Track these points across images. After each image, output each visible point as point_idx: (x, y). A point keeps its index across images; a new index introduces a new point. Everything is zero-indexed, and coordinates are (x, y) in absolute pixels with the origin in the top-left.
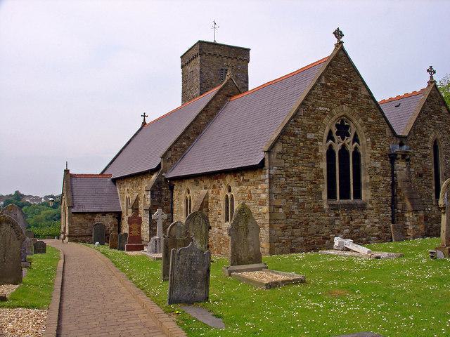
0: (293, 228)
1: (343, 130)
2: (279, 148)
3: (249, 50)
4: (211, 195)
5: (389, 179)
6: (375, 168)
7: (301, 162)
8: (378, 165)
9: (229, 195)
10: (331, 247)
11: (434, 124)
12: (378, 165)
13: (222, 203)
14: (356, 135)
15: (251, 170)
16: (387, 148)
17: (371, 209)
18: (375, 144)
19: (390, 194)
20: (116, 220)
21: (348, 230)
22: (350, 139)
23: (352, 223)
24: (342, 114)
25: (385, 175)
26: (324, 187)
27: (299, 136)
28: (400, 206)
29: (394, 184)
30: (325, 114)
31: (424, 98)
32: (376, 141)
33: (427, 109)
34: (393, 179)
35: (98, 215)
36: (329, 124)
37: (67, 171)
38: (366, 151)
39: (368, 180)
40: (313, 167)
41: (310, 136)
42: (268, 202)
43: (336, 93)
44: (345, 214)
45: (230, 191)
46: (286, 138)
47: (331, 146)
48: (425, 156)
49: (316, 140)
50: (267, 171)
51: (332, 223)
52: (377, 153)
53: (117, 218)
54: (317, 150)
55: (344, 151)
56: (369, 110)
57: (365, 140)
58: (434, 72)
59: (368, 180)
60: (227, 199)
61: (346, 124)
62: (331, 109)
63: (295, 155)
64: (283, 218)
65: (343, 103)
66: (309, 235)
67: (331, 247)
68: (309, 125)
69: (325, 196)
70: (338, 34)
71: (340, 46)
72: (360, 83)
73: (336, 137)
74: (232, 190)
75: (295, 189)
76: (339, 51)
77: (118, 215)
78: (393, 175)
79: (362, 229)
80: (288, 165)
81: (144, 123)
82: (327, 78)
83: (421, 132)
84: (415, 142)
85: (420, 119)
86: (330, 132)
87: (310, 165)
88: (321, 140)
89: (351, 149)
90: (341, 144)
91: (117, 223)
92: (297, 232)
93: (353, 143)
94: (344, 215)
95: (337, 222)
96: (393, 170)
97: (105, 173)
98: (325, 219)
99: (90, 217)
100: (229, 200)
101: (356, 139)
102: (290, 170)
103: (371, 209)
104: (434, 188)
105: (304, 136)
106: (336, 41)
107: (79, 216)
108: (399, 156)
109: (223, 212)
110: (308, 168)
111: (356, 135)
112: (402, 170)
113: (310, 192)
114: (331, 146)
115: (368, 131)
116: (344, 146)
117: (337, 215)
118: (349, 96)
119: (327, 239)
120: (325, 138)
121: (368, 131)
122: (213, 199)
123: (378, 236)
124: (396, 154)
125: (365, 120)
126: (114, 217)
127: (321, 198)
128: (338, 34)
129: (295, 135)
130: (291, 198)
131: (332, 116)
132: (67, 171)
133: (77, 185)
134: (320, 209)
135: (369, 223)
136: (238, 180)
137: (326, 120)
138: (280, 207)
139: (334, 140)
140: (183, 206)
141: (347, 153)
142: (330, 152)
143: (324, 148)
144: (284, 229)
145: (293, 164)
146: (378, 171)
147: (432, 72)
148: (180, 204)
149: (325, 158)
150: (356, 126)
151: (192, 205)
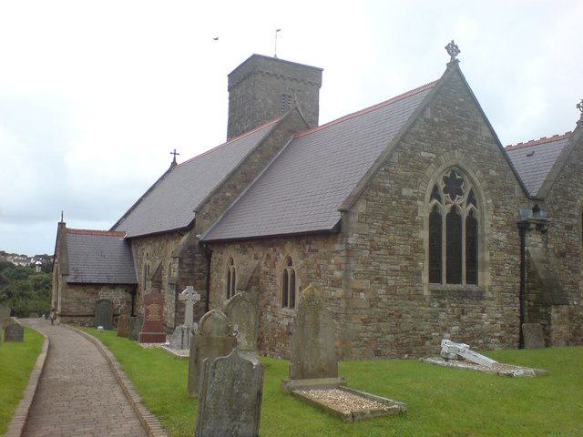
0: (380, 321)
3: (321, 70)
5: (517, 258)
6: (497, 242)
8: (502, 237)
12: (502, 237)
13: (279, 281)
14: (471, 193)
17: (492, 299)
20: (129, 296)
22: (464, 199)
30: (428, 162)
36: (435, 177)
37: (62, 225)
40: (410, 236)
44: (455, 305)
45: (290, 264)
49: (415, 199)
52: (501, 220)
53: (131, 293)
54: (415, 213)
57: (486, 201)
61: (458, 177)
62: (438, 155)
63: (385, 218)
70: (452, 49)
71: (453, 67)
73: (444, 196)
74: (294, 263)
75: (383, 267)
79: (477, 327)
81: (174, 164)
86: (436, 188)
88: (422, 199)
89: (464, 212)
90: (450, 205)
92: (385, 327)
93: (467, 205)
95: (442, 316)
96: (523, 245)
97: (118, 230)
102: (376, 239)
103: (492, 299)
106: (448, 58)
108: (533, 226)
109: (280, 293)
113: (404, 271)
114: (435, 207)
116: (454, 208)
117: (442, 306)
120: (428, 196)
126: (126, 291)
127: (420, 281)
129: (385, 190)
130: (377, 279)
132: (62, 225)
134: (418, 296)
137: (429, 171)
140: (224, 281)
141: (439, 217)
146: (502, 245)
149: (426, 224)
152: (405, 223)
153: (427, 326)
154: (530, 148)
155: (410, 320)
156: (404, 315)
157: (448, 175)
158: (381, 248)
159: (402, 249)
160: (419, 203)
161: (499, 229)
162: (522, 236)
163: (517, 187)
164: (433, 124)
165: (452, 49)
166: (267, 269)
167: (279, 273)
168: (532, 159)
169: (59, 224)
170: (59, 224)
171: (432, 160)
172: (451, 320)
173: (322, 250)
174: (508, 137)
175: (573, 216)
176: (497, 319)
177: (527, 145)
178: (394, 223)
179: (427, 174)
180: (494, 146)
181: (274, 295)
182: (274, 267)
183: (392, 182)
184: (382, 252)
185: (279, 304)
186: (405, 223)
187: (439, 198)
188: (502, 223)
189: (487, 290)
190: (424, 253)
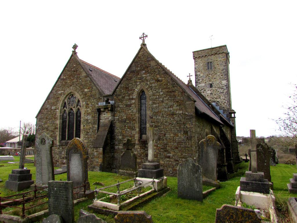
2: (40, 117)
6: (87, 120)
7: (49, 121)
11: (141, 79)
15: (139, 206)
25: (94, 124)
27: (48, 109)
32: (89, 102)
33: (134, 68)
49: (56, 109)
70: (144, 37)
71: (144, 45)
89: (75, 110)
96: (99, 119)
102: (44, 126)
104: (137, 130)
106: (141, 42)
117: (63, 149)
119: (57, 161)
141: (73, 114)
146: (89, 121)
152: (52, 119)
159: (51, 128)
162: (99, 115)
165: (75, 47)
178: (49, 119)
188: (90, 111)
190: (58, 129)
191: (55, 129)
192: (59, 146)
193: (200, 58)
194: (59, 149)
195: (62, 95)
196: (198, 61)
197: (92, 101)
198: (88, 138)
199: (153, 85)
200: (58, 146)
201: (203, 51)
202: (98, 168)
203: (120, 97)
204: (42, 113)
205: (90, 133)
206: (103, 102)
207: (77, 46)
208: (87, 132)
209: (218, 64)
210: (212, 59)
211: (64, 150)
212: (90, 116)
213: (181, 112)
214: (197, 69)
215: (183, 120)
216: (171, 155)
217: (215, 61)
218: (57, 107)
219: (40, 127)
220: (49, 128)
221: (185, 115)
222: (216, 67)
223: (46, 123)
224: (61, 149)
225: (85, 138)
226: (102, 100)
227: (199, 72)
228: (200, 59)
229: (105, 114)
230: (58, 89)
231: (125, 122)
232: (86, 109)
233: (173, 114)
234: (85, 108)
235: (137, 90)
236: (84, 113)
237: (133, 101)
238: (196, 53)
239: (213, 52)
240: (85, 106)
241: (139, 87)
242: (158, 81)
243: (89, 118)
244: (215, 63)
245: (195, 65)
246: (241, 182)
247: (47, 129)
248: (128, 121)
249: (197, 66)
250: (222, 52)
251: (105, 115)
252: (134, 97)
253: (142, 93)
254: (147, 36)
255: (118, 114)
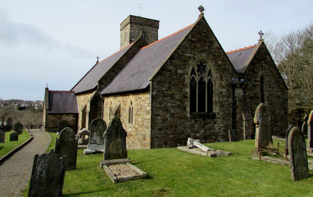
0: (167, 129)
1: (201, 67)
2: (159, 79)
3: (159, 21)
4: (122, 106)
5: (231, 100)
6: (222, 93)
7: (173, 87)
8: (224, 90)
9: (131, 107)
10: (185, 144)
11: (262, 66)
12: (224, 90)
13: (127, 111)
16: (230, 80)
17: (219, 118)
18: (222, 77)
19: (231, 109)
20: (75, 118)
21: (203, 131)
22: (206, 74)
23: (206, 126)
24: (201, 58)
25: (228, 97)
26: (188, 104)
28: (238, 116)
29: (234, 103)
30: (190, 58)
31: (255, 51)
34: (233, 100)
35: (64, 115)
36: (192, 64)
37: (47, 89)
38: (217, 82)
39: (217, 100)
40: (181, 90)
41: (179, 71)
42: (150, 112)
43: (198, 45)
44: (202, 121)
45: (131, 104)
46: (164, 72)
47: (193, 78)
48: (255, 86)
49: (184, 74)
50: (151, 93)
51: (193, 126)
52: (224, 83)
53: (75, 117)
54: (184, 80)
55: (202, 82)
56: (219, 56)
57: (215, 75)
58: (263, 34)
59: (217, 100)
60: (130, 109)
61: (204, 64)
62: (194, 55)
63: (170, 83)
64: (160, 122)
65: (202, 52)
66: (177, 134)
67: (185, 144)
68: (179, 65)
69: (188, 109)
70: (201, 9)
72: (214, 40)
74: (133, 104)
75: (169, 105)
76: (201, 19)
77: (76, 115)
78: (234, 97)
79: (212, 130)
80: (165, 89)
81: (98, 62)
82: (193, 37)
83: (253, 71)
84: (249, 77)
85: (253, 63)
86: (193, 69)
87: (179, 89)
88: (187, 74)
89: (206, 80)
90: (200, 77)
91: (75, 120)
92: (169, 132)
94: (201, 121)
95: (196, 126)
96: (234, 94)
97: (72, 91)
98: (188, 124)
99: (59, 116)
100: (131, 110)
101: (210, 73)
102: (166, 92)
103: (219, 118)
105: (176, 71)
106: (199, 13)
107: (52, 115)
108: (238, 85)
109: (128, 117)
110: (178, 92)
111: (210, 71)
112: (240, 94)
113: (179, 106)
115: (218, 69)
116: (202, 78)
117: (196, 121)
118: (207, 48)
120: (189, 74)
121: (218, 69)
122: (123, 108)
123: (223, 135)
124: (236, 84)
125: (216, 63)
126: (74, 116)
127: (186, 111)
128: (201, 9)
129: (170, 71)
130: (166, 110)
131: (195, 59)
132: (47, 89)
133: (56, 98)
134: (185, 117)
135: (219, 125)
136: (136, 97)
137: (190, 62)
138: (158, 115)
139: (195, 75)
140: (108, 111)
142: (193, 80)
143: (189, 79)
144: (160, 129)
145: (167, 89)
146: (224, 94)
147: (261, 34)
148: (107, 110)
149: (189, 85)
150: (210, 66)
151: (113, 110)
152: (179, 85)
153: (189, 131)
154: (241, 52)
155: (181, 128)
156: (178, 126)
157: (199, 64)
158: (168, 97)
160: (186, 76)
161: (223, 87)
163: (231, 68)
164: (193, 42)
166: (123, 106)
167: (127, 108)
168: (240, 56)
169: (46, 88)
170: (46, 88)
171: (191, 57)
172: (200, 128)
173: (143, 98)
174: (227, 49)
175: (257, 81)
176: (222, 127)
177: (238, 51)
178: (174, 85)
179: (189, 63)
180: (221, 51)
181: (126, 118)
182: (126, 105)
183: (173, 67)
184: (168, 98)
185: (127, 122)
186: (179, 85)
187: (211, 76)
188: (224, 84)
189: (217, 114)
191: (184, 98)
192: (191, 118)
193: (136, 24)
194: (190, 122)
195: (192, 59)
196: (134, 26)
197: (227, 75)
198: (224, 110)
199: (269, 74)
200: (189, 119)
201: (140, 19)
202: (250, 137)
203: (249, 77)
204: (162, 75)
205: (225, 106)
206: (236, 78)
207: (201, 7)
208: (223, 105)
209: (151, 36)
210: (146, 30)
211: (197, 123)
212: (225, 89)
213: (283, 96)
214: (132, 34)
215: (283, 102)
216: (278, 124)
217: (149, 33)
218: (185, 72)
219: (159, 93)
220: (175, 96)
221: (285, 98)
222: (149, 38)
223: (169, 89)
224: (193, 121)
225: (220, 111)
226: (236, 76)
227: (134, 38)
228: (136, 26)
229: (237, 90)
230: (185, 51)
231: (253, 99)
232: (220, 82)
233: (279, 97)
234: (219, 80)
235: (260, 74)
236: (219, 86)
237: (258, 83)
238: (133, 18)
239: (149, 23)
240: (219, 78)
241: (261, 73)
242: (271, 72)
243: (223, 91)
244: (149, 34)
245: (130, 30)
246: (151, 148)
247: (172, 97)
248: (255, 99)
249: (132, 31)
250: (156, 26)
251: (238, 91)
252: (258, 80)
253: (262, 78)
254: (261, 32)
255: (248, 92)
